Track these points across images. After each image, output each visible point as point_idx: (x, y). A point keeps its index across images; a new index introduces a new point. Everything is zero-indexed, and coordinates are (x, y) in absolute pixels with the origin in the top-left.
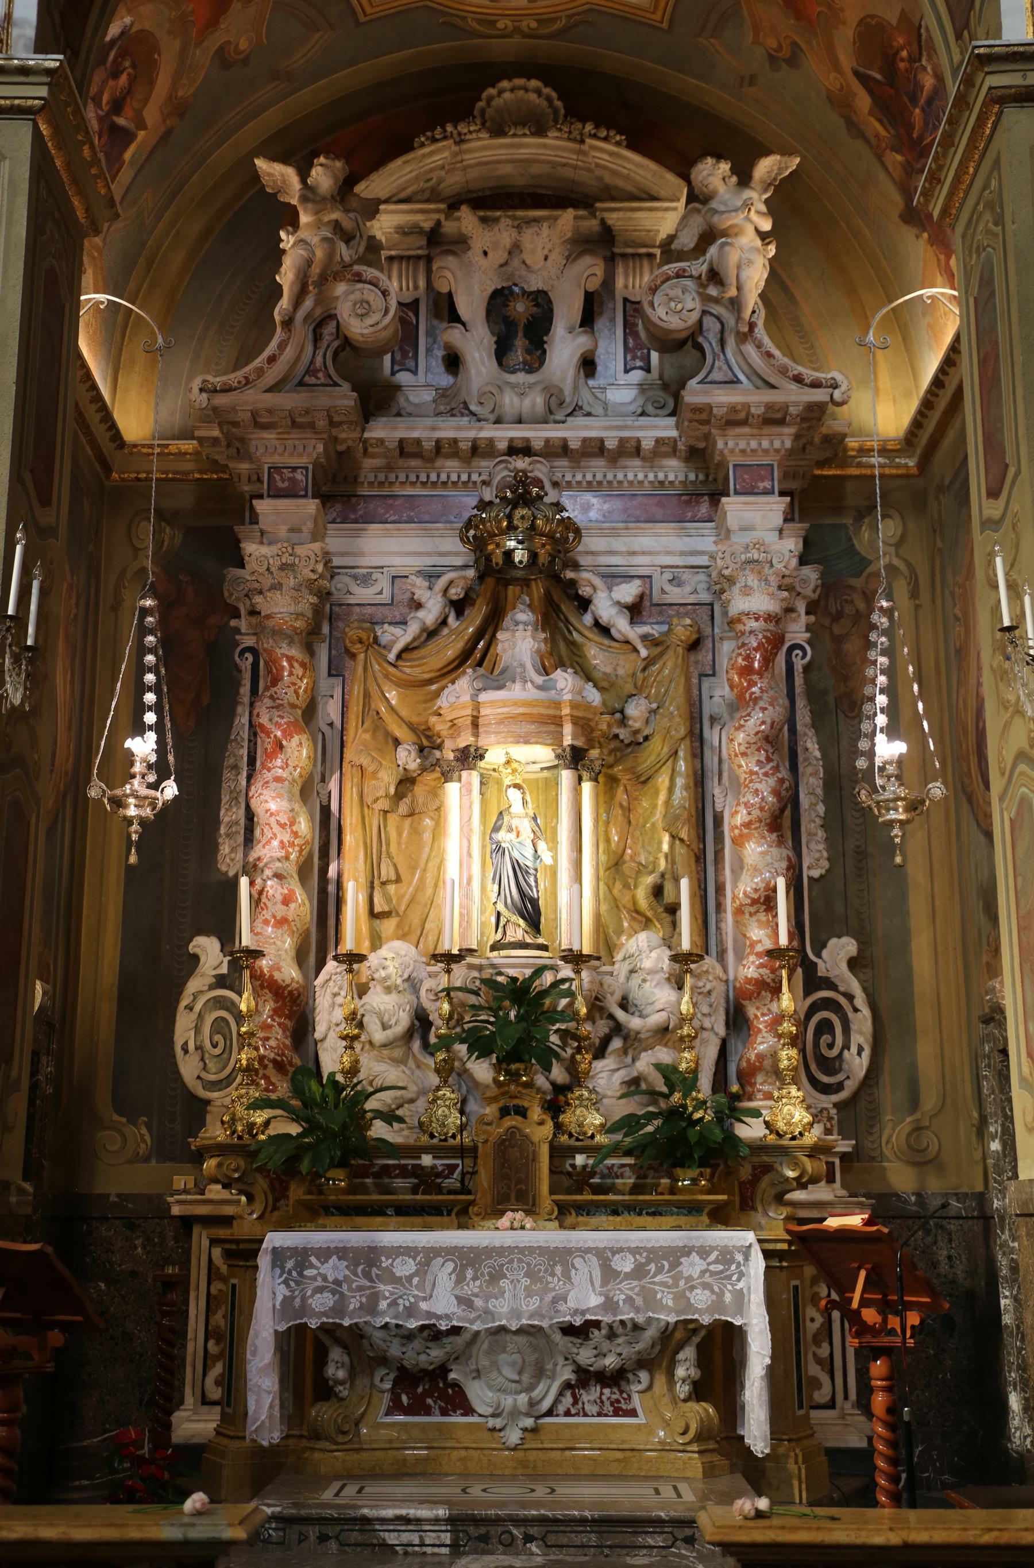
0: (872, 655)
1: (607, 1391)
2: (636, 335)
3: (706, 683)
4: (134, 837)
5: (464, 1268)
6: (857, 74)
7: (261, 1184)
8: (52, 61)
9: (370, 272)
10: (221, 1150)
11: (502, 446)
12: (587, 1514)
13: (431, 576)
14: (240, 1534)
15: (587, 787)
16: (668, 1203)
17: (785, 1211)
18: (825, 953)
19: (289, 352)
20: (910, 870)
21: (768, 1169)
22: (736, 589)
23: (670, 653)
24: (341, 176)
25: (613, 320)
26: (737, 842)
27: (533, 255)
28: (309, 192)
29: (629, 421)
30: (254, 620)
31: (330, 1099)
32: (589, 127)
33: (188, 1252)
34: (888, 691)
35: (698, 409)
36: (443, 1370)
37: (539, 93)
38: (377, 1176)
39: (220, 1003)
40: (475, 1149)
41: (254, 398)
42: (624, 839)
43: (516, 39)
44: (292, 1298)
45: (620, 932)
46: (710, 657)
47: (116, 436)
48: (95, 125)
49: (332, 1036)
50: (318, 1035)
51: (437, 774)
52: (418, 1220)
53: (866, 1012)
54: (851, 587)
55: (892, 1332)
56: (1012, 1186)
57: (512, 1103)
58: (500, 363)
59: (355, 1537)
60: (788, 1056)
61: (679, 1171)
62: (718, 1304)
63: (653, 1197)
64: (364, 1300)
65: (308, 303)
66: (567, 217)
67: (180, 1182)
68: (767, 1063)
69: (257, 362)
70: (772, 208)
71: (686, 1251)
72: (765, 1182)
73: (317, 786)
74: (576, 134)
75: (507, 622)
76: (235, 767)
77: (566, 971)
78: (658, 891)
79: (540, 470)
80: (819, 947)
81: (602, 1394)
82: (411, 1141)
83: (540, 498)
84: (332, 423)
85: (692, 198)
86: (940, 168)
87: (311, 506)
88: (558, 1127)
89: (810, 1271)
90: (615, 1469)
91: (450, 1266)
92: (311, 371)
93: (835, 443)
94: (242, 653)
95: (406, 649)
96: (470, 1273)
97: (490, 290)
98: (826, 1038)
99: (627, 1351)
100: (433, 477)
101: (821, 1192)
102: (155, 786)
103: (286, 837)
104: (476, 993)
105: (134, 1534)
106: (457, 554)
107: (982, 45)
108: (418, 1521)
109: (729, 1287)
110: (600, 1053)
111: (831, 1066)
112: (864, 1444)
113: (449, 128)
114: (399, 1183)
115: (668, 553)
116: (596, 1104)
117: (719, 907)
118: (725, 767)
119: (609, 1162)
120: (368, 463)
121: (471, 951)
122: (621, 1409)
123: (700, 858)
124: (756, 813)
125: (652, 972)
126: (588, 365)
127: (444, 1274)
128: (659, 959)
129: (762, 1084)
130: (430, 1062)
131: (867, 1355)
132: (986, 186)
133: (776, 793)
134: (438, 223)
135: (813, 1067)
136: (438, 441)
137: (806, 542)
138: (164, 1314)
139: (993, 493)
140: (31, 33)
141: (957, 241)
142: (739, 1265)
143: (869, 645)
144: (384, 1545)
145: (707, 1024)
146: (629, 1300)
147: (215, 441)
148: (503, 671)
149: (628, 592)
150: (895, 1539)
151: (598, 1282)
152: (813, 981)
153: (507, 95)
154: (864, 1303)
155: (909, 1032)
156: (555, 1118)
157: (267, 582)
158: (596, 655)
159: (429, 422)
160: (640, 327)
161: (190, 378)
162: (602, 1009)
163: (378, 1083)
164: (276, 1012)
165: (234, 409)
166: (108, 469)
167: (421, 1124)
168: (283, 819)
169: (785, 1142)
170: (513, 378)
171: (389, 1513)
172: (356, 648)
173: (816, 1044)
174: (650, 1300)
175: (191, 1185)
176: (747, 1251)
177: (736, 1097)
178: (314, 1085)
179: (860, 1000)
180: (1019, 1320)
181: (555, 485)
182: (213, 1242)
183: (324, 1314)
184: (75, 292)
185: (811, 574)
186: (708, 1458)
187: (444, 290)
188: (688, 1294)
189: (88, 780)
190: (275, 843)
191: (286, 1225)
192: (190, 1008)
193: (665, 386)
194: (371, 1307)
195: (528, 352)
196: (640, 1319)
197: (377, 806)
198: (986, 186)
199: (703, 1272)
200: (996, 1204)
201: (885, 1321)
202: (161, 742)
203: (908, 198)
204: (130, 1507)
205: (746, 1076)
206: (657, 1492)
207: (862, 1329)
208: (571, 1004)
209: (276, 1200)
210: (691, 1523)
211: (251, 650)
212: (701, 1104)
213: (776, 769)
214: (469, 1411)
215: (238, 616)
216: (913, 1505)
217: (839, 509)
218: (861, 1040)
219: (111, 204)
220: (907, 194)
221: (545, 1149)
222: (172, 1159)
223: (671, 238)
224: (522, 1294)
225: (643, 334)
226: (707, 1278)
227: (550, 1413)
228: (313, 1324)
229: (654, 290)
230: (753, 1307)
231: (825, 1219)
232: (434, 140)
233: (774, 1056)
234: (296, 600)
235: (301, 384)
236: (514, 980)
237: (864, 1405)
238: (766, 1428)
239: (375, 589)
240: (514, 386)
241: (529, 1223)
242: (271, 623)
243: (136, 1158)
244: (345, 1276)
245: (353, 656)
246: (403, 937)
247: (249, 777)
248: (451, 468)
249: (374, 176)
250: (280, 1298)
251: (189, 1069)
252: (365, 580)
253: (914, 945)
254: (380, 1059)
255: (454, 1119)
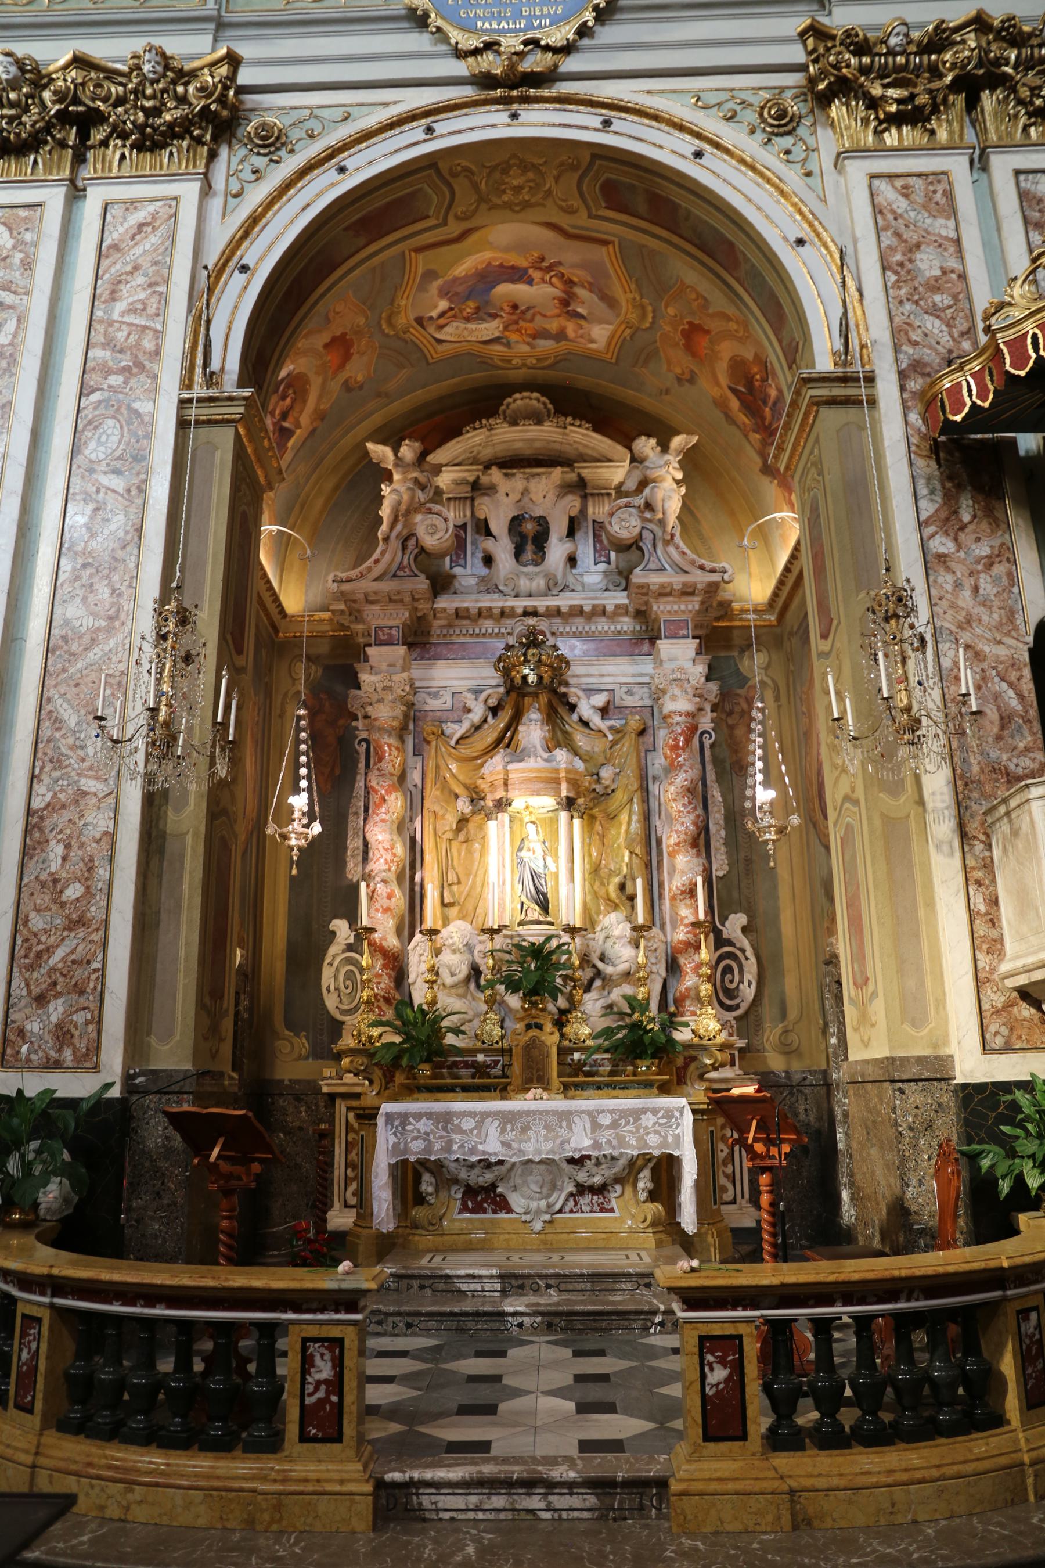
0: (753, 736)
1: (595, 1198)
2: (601, 542)
3: (650, 756)
4: (295, 858)
5: (505, 1124)
6: (730, 388)
7: (377, 1074)
8: (247, 392)
9: (436, 508)
10: (353, 1052)
11: (520, 611)
12: (585, 1271)
13: (477, 692)
14: (373, 1285)
15: (577, 822)
16: (632, 1081)
17: (705, 1085)
18: (727, 924)
19: (388, 557)
20: (779, 871)
21: (694, 1059)
22: (667, 697)
23: (627, 738)
24: (419, 452)
25: (587, 533)
26: (672, 855)
27: (537, 497)
28: (399, 462)
29: (598, 594)
30: (367, 721)
31: (419, 1020)
32: (569, 419)
33: (333, 1115)
34: (764, 759)
35: (641, 587)
36: (493, 1186)
37: (538, 400)
38: (450, 1067)
39: (349, 961)
40: (510, 1050)
41: (366, 585)
42: (600, 854)
43: (524, 370)
45: (599, 913)
47: (282, 611)
48: (270, 428)
49: (420, 981)
50: (410, 981)
51: (482, 816)
52: (476, 1095)
53: (753, 959)
55: (773, 1157)
56: (845, 1065)
57: (533, 1021)
58: (517, 560)
59: (442, 1286)
60: (706, 989)
61: (638, 1062)
62: (664, 1143)
63: (623, 1078)
65: (399, 527)
66: (557, 473)
67: (327, 1072)
68: (692, 993)
69: (368, 564)
70: (683, 465)
71: (644, 1111)
72: (692, 1067)
73: (407, 824)
74: (561, 424)
75: (525, 719)
76: (356, 814)
77: (566, 938)
78: (622, 887)
79: (543, 625)
80: (724, 919)
82: (471, 1046)
83: (544, 642)
84: (414, 599)
85: (633, 460)
86: (783, 442)
87: (402, 650)
88: (562, 1035)
89: (720, 1121)
90: (601, 1244)
91: (497, 1123)
92: (400, 568)
93: (725, 609)
94: (360, 742)
95: (462, 738)
96: (509, 1127)
97: (510, 517)
98: (728, 977)
99: (607, 1173)
100: (477, 631)
101: (727, 1073)
102: (307, 826)
103: (389, 857)
104: (509, 953)
105: (308, 1285)
106: (493, 678)
107: (805, 372)
108: (480, 1277)
110: (588, 989)
111: (731, 994)
112: (754, 1225)
113: (484, 421)
114: (463, 1072)
115: (625, 675)
116: (586, 1021)
117: (661, 896)
118: (663, 808)
119: (595, 1057)
120: (436, 623)
121: (505, 926)
123: (648, 865)
124: (683, 836)
125: (619, 938)
126: (572, 561)
127: (492, 1128)
128: (624, 929)
129: (689, 1006)
130: (482, 996)
131: (755, 1172)
132: (811, 453)
133: (695, 824)
134: (478, 477)
135: (721, 995)
136: (480, 609)
137: (710, 667)
138: (321, 1153)
139: (824, 636)
140: (235, 377)
141: (796, 485)
143: (750, 730)
144: (460, 1292)
145: (654, 969)
146: (609, 1142)
147: (342, 612)
148: (523, 750)
149: (600, 700)
150: (776, 1281)
151: (589, 1131)
152: (720, 941)
153: (519, 402)
154: (755, 1140)
155: (780, 973)
156: (560, 1030)
157: (375, 697)
158: (581, 739)
159: (474, 597)
160: (604, 537)
161: (327, 574)
162: (588, 961)
163: (449, 1010)
164: (384, 966)
165: (353, 593)
166: (276, 631)
167: (476, 1035)
168: (387, 845)
169: (704, 1042)
170: (525, 569)
171: (462, 1272)
172: (431, 738)
173: (723, 981)
174: (622, 1141)
175: (334, 1074)
176: (681, 1110)
177: (673, 1015)
178: (409, 1011)
179: (749, 952)
180: (849, 1147)
181: (553, 634)
182: (349, 1109)
184: (258, 524)
185: (714, 687)
186: (658, 1236)
187: (482, 517)
189: (266, 823)
190: (382, 861)
191: (394, 1098)
192: (331, 964)
193: (620, 573)
194: (448, 1149)
195: (535, 553)
196: (616, 1153)
197: (445, 836)
198: (811, 453)
199: (655, 1124)
200: (834, 1076)
201: (768, 1150)
202: (311, 799)
203: (764, 457)
204: (306, 1269)
205: (679, 1002)
206: (627, 1257)
207: (754, 1155)
208: (569, 959)
209: (387, 1083)
210: (650, 1275)
211: (365, 740)
212: (652, 1020)
213: (695, 809)
214: (510, 1210)
215: (357, 719)
216: (785, 1261)
217: (729, 647)
218: (750, 977)
219: (280, 472)
220: (764, 457)
221: (554, 1051)
222: (322, 1058)
223: (621, 484)
224: (542, 1139)
225: (605, 541)
226: (657, 1127)
227: (560, 1211)
228: (412, 1159)
229: (612, 515)
230: (686, 1145)
231: (730, 1090)
232: (475, 429)
233: (697, 988)
234: (392, 709)
235: (395, 576)
236: (533, 944)
237: (755, 1201)
238: (695, 1217)
239: (442, 701)
240: (526, 574)
241: (545, 1095)
242: (377, 723)
243: (300, 1058)
245: (429, 743)
246: (463, 918)
247: (365, 820)
248: (488, 625)
249: (438, 451)
250: (391, 1143)
251: (331, 1002)
252: (436, 695)
253: (782, 917)
254: (450, 995)
255: (497, 1032)
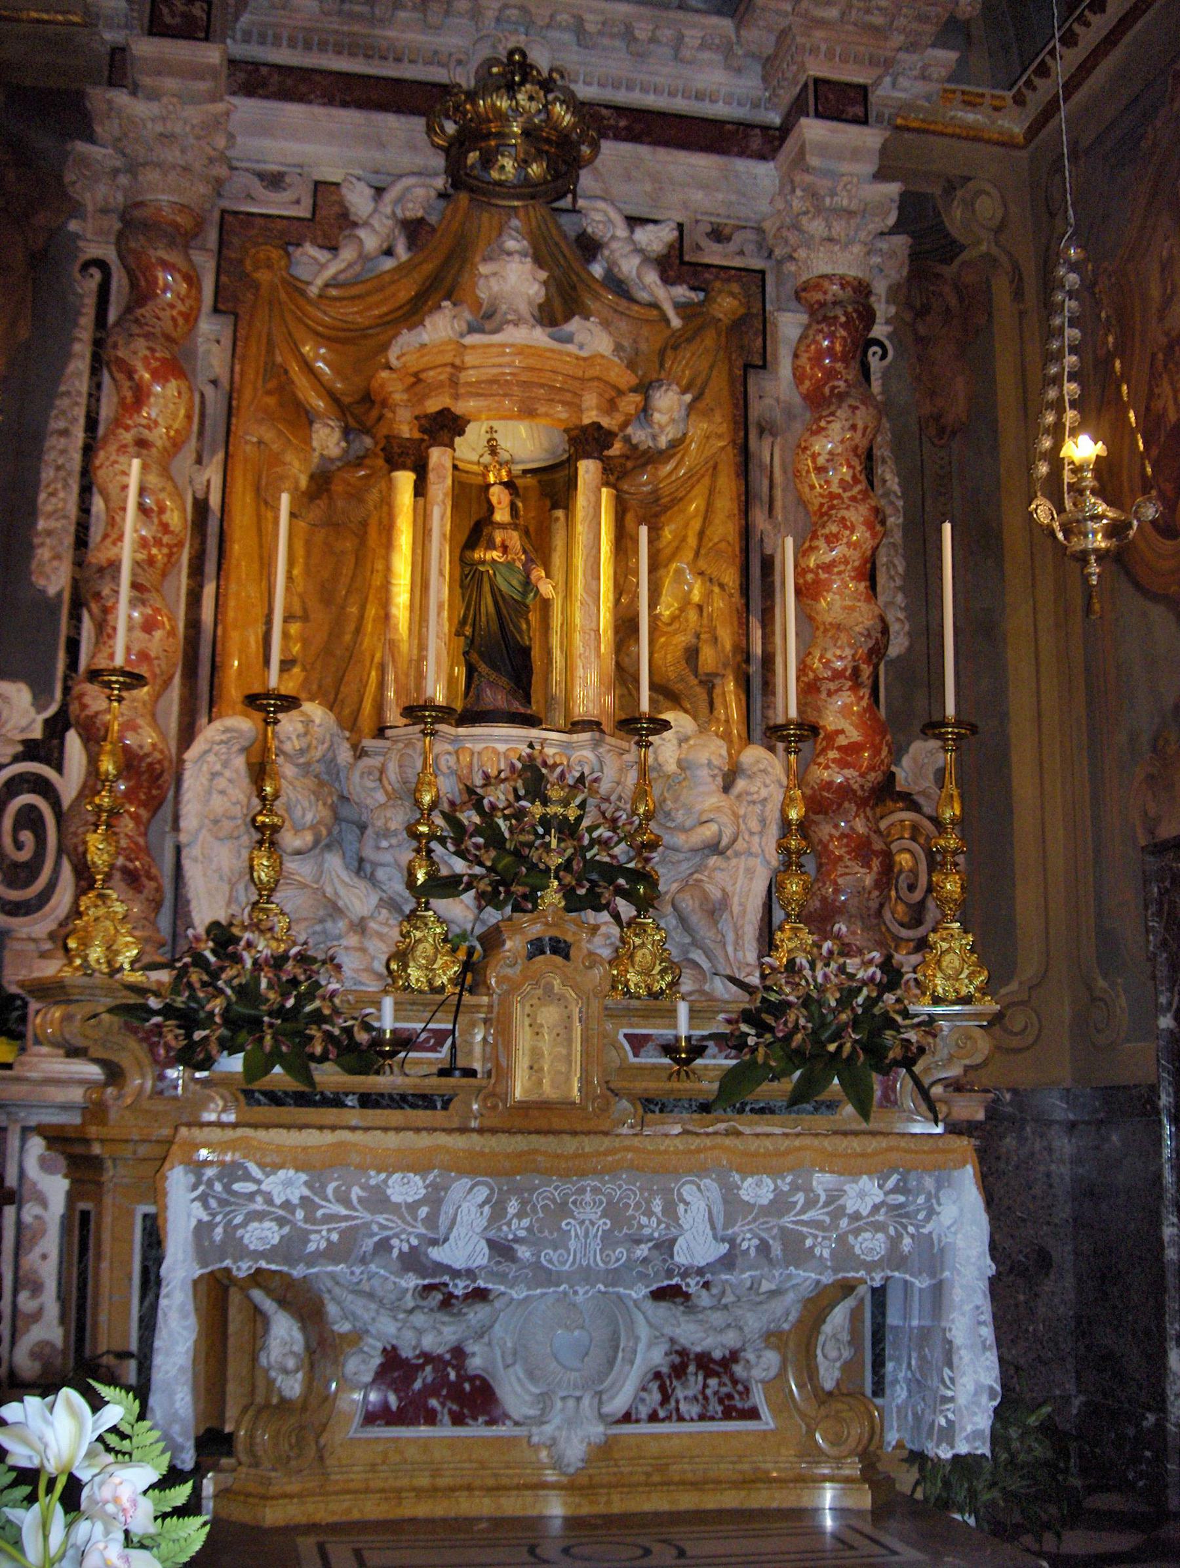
44: (211, 1226)
46: (759, 342)
54: (938, 276)
64: (335, 1237)
81: (705, 1386)
91: (482, 1193)
96: (513, 1207)
109: (911, 1229)
122: (734, 1408)
142: (929, 1194)
149: (655, 238)
183: (262, 1255)
188: (851, 1238)
199: (876, 1208)
227: (627, 1418)
244: (302, 1198)
